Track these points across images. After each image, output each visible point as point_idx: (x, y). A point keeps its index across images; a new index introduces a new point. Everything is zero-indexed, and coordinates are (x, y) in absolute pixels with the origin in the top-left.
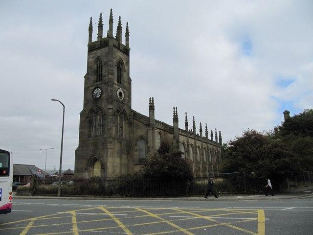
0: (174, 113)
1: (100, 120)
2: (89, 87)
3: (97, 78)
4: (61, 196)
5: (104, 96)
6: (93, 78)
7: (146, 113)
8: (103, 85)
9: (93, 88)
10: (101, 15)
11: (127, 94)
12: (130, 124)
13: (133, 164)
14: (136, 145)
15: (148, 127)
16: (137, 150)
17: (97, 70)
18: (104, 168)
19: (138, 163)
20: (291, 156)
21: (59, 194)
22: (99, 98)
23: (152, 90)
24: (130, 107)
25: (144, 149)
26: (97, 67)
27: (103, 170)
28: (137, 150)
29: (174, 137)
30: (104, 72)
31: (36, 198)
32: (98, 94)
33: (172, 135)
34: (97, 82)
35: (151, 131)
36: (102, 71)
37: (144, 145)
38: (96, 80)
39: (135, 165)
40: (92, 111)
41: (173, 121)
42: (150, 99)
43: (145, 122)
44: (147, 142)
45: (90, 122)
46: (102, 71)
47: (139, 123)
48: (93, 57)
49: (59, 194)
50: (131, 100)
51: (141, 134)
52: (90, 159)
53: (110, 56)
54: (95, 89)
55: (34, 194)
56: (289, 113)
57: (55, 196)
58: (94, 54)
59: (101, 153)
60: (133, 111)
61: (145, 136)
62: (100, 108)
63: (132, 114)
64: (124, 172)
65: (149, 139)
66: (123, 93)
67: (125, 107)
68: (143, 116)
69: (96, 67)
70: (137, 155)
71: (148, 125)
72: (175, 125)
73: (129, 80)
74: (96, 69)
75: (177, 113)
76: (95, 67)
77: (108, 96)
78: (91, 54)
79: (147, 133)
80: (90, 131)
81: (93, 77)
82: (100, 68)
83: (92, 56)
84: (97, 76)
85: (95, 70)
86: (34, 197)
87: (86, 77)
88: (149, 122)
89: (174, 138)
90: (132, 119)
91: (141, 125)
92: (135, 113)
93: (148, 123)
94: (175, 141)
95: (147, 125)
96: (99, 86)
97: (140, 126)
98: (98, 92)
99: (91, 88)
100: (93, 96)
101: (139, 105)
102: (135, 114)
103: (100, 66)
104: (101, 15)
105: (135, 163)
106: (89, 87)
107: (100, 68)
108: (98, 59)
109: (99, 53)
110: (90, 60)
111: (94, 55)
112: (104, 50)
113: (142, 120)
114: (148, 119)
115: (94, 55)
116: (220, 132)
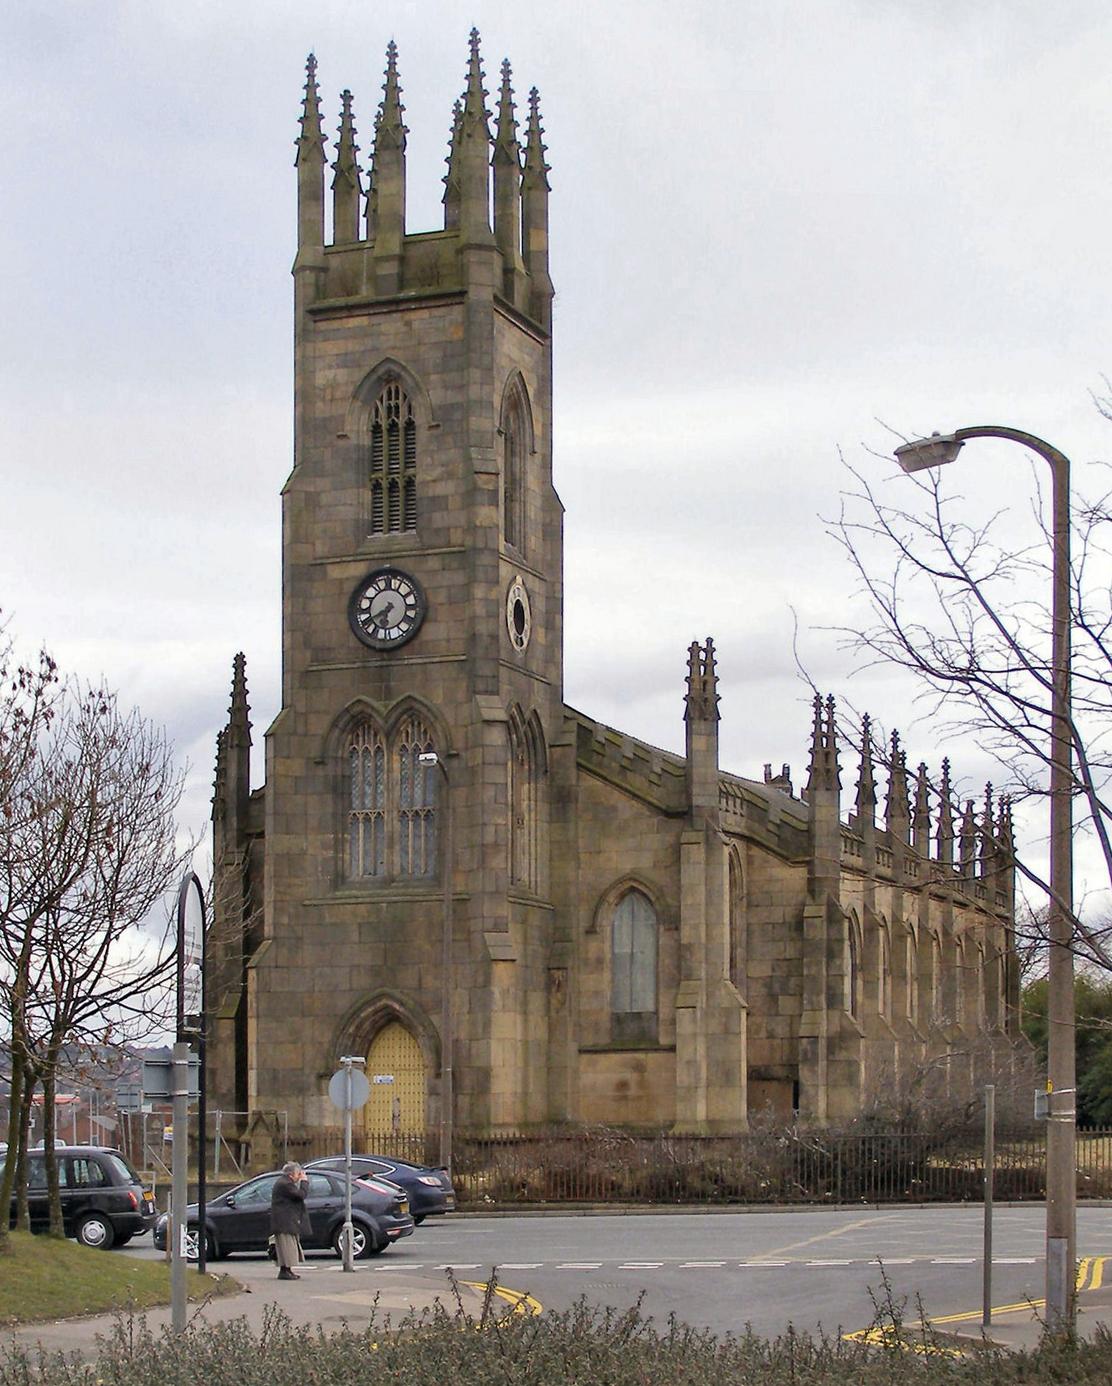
0: (817, 722)
2: (320, 565)
3: (375, 501)
5: (433, 632)
6: (350, 502)
7: (661, 727)
8: (433, 563)
9: (359, 570)
10: (392, 54)
11: (540, 604)
12: (561, 801)
14: (591, 931)
15: (675, 824)
17: (375, 449)
19: (604, 1040)
20: (438, 879)
24: (556, 691)
25: (646, 956)
26: (376, 429)
28: (600, 961)
29: (812, 886)
30: (432, 472)
32: (392, 617)
33: (801, 873)
34: (374, 527)
35: (696, 854)
36: (409, 464)
37: (646, 938)
38: (367, 516)
40: (357, 722)
41: (687, 717)
43: (655, 795)
44: (671, 920)
46: (410, 454)
47: (617, 798)
48: (346, 361)
51: (626, 866)
52: (355, 1014)
54: (368, 581)
59: (429, 981)
60: (574, 715)
61: (660, 877)
62: (412, 713)
63: (572, 739)
65: (687, 901)
66: (525, 605)
67: (539, 700)
68: (642, 754)
70: (597, 993)
71: (680, 814)
72: (699, 743)
73: (553, 506)
74: (366, 440)
75: (831, 723)
76: (358, 427)
77: (473, 638)
79: (676, 852)
80: (338, 845)
81: (350, 495)
82: (394, 434)
83: (332, 348)
84: (377, 487)
85: (358, 447)
87: (298, 502)
88: (678, 793)
89: (812, 892)
90: (573, 772)
91: (626, 807)
92: (585, 729)
93: (674, 802)
95: (669, 814)
98: (391, 602)
99: (335, 572)
102: (589, 738)
103: (393, 426)
104: (392, 54)
105: (589, 1040)
106: (320, 565)
107: (394, 434)
108: (386, 384)
110: (321, 378)
111: (352, 346)
112: (432, 325)
113: (636, 782)
114: (680, 774)
115: (352, 346)
116: (534, 98)
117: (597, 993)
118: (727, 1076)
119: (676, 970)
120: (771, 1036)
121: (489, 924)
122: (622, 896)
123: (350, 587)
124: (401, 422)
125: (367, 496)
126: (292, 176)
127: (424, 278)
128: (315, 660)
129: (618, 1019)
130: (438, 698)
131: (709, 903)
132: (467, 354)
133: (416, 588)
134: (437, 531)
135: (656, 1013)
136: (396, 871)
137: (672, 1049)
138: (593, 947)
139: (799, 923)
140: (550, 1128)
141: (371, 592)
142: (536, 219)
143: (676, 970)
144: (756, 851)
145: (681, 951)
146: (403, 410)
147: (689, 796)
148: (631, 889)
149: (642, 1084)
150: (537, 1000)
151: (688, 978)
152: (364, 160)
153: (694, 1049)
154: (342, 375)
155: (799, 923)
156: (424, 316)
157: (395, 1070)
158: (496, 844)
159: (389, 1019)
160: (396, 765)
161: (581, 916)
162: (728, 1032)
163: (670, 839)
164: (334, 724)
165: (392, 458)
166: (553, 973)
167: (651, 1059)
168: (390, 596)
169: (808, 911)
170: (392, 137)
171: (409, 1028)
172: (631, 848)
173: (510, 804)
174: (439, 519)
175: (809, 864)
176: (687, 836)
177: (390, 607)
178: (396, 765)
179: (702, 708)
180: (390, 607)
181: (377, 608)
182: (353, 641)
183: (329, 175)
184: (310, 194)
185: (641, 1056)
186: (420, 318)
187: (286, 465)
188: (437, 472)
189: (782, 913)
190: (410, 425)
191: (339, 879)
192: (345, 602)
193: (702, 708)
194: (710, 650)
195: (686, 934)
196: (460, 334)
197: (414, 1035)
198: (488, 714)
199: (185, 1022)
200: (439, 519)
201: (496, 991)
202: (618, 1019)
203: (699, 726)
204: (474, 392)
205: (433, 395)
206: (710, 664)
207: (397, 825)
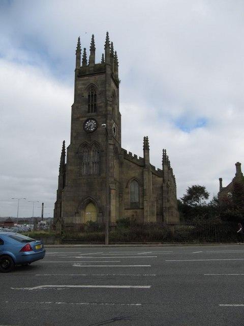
0: (163, 154)
1: (93, 156)
2: (78, 118)
3: (89, 108)
4: (109, 244)
7: (140, 154)
8: (99, 117)
9: (86, 119)
13: (124, 208)
15: (142, 168)
16: (128, 193)
18: (102, 211)
19: (129, 207)
21: (107, 240)
22: (94, 130)
23: (139, 127)
26: (89, 96)
27: (101, 214)
28: (128, 193)
29: (164, 180)
30: (100, 102)
31: (54, 247)
34: (89, 112)
37: (137, 188)
38: (87, 110)
39: (125, 209)
40: (85, 145)
41: (144, 149)
42: (145, 138)
45: (81, 158)
46: (95, 100)
48: (84, 84)
49: (107, 240)
50: (120, 137)
53: (107, 85)
54: (87, 120)
55: (64, 241)
56: (240, 164)
57: (102, 244)
58: (85, 80)
64: (118, 218)
65: (145, 181)
69: (87, 95)
70: (128, 199)
73: (119, 115)
74: (87, 97)
75: (166, 154)
76: (86, 95)
78: (80, 80)
79: (142, 174)
83: (81, 82)
84: (89, 105)
86: (115, 245)
93: (142, 164)
94: (166, 185)
96: (93, 117)
97: (132, 166)
98: (91, 125)
99: (81, 119)
100: (86, 131)
101: (131, 144)
103: (92, 95)
107: (92, 97)
108: (92, 87)
109: (92, 80)
110: (80, 87)
111: (83, 82)
112: (100, 78)
117: (128, 199)
118: (153, 213)
119: (143, 194)
120: (168, 201)
121: (110, 182)
122: (132, 181)
123: (84, 122)
124: (94, 94)
125: (87, 107)
126: (75, 56)
127: (100, 70)
128: (77, 135)
129: (132, 203)
130: (100, 140)
131: (149, 182)
132: (105, 83)
133: (96, 122)
134: (100, 112)
135: (139, 202)
136: (92, 173)
137: (143, 209)
138: (127, 190)
139: (162, 187)
140: (124, 223)
141: (88, 123)
142: (116, 70)
143: (143, 194)
144: (154, 176)
145: (143, 190)
146: (94, 92)
147: (145, 163)
148: (135, 179)
149: (136, 215)
150: (117, 198)
151: (146, 195)
152: (88, 59)
153: (147, 208)
154: (83, 86)
155: (162, 187)
156: (97, 83)
157: (90, 212)
158: (111, 167)
159: (90, 202)
160: (92, 154)
161: (125, 184)
162: (153, 205)
163: (141, 170)
164: (80, 146)
165: (92, 101)
166: (120, 195)
167: (138, 211)
168: (91, 123)
169: (164, 185)
170: (93, 49)
171: (94, 204)
172: (135, 173)
173: (114, 163)
174: (100, 110)
175: (163, 177)
176: (144, 170)
177: (91, 125)
178: (92, 154)
179: (146, 148)
180: (91, 125)
181: (89, 125)
182: (84, 131)
183: (82, 60)
184: (78, 58)
185: (136, 210)
186: (97, 77)
187: (73, 102)
188: (100, 102)
189: (159, 186)
190: (95, 95)
191: (81, 175)
192: (82, 124)
193: (146, 148)
194: (147, 138)
195: (145, 187)
196: (104, 79)
197: (95, 205)
198: (110, 143)
199: (90, 215)
200: (100, 110)
201: (112, 195)
202: (132, 203)
203: (146, 151)
204: (107, 88)
205: (100, 89)
206: (147, 141)
207: (92, 165)
